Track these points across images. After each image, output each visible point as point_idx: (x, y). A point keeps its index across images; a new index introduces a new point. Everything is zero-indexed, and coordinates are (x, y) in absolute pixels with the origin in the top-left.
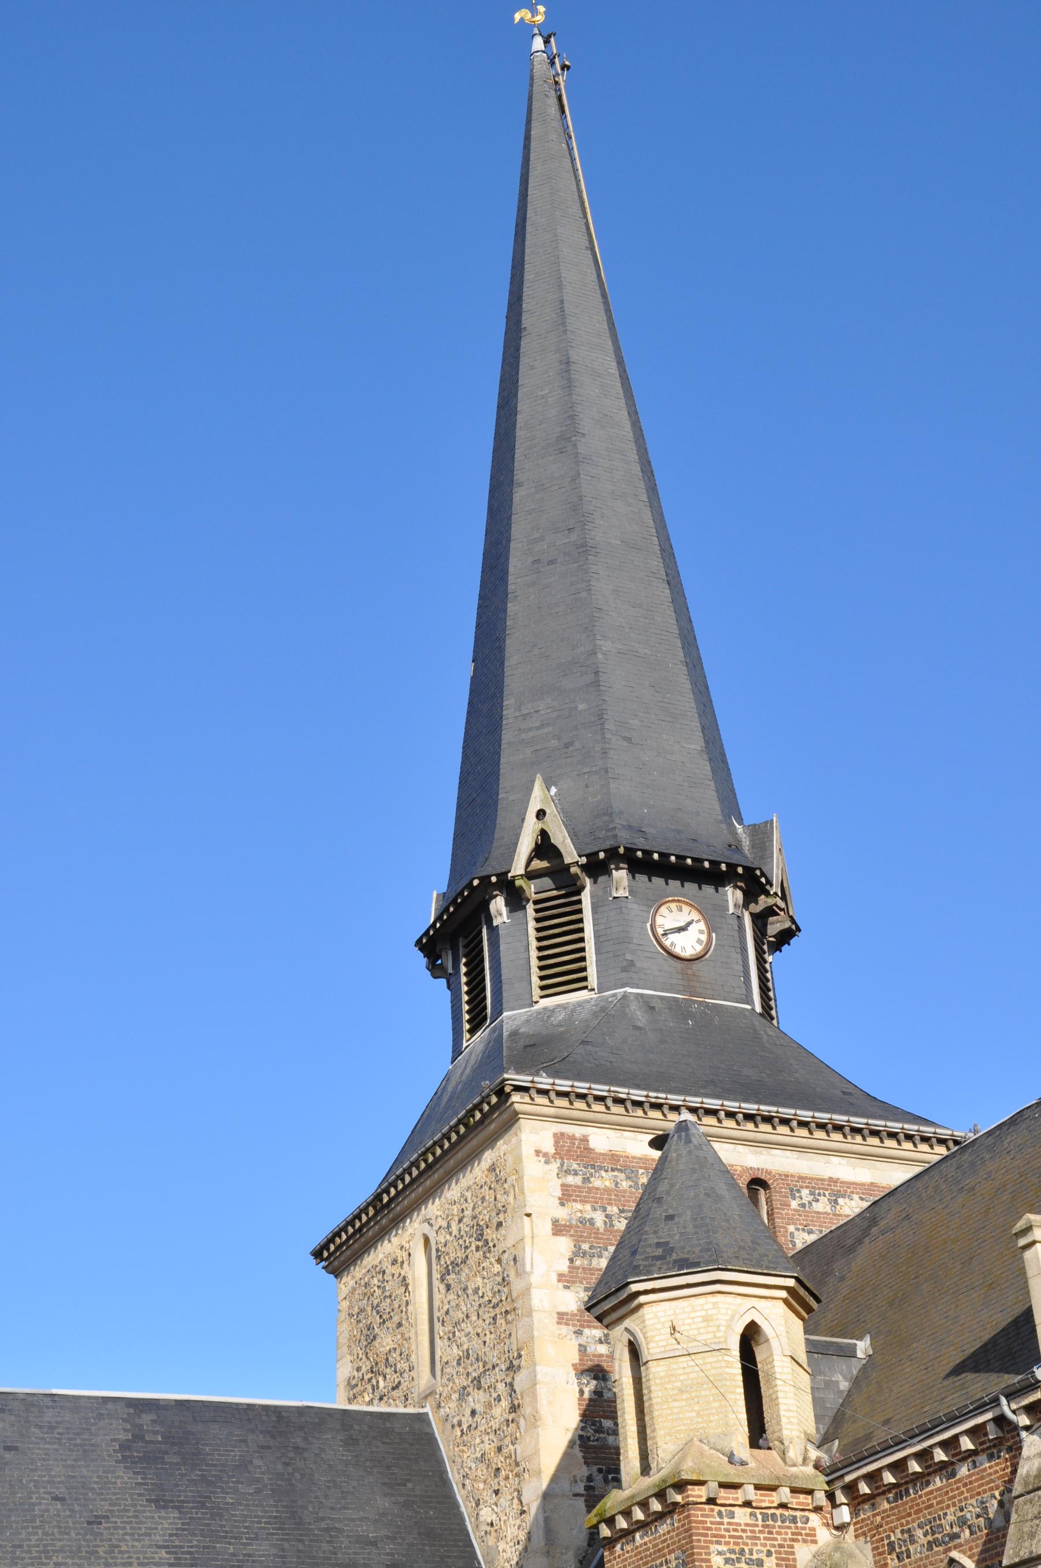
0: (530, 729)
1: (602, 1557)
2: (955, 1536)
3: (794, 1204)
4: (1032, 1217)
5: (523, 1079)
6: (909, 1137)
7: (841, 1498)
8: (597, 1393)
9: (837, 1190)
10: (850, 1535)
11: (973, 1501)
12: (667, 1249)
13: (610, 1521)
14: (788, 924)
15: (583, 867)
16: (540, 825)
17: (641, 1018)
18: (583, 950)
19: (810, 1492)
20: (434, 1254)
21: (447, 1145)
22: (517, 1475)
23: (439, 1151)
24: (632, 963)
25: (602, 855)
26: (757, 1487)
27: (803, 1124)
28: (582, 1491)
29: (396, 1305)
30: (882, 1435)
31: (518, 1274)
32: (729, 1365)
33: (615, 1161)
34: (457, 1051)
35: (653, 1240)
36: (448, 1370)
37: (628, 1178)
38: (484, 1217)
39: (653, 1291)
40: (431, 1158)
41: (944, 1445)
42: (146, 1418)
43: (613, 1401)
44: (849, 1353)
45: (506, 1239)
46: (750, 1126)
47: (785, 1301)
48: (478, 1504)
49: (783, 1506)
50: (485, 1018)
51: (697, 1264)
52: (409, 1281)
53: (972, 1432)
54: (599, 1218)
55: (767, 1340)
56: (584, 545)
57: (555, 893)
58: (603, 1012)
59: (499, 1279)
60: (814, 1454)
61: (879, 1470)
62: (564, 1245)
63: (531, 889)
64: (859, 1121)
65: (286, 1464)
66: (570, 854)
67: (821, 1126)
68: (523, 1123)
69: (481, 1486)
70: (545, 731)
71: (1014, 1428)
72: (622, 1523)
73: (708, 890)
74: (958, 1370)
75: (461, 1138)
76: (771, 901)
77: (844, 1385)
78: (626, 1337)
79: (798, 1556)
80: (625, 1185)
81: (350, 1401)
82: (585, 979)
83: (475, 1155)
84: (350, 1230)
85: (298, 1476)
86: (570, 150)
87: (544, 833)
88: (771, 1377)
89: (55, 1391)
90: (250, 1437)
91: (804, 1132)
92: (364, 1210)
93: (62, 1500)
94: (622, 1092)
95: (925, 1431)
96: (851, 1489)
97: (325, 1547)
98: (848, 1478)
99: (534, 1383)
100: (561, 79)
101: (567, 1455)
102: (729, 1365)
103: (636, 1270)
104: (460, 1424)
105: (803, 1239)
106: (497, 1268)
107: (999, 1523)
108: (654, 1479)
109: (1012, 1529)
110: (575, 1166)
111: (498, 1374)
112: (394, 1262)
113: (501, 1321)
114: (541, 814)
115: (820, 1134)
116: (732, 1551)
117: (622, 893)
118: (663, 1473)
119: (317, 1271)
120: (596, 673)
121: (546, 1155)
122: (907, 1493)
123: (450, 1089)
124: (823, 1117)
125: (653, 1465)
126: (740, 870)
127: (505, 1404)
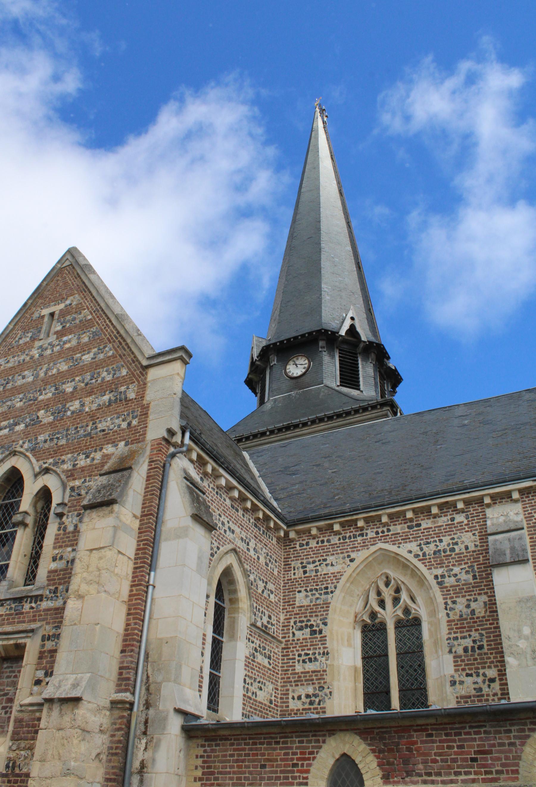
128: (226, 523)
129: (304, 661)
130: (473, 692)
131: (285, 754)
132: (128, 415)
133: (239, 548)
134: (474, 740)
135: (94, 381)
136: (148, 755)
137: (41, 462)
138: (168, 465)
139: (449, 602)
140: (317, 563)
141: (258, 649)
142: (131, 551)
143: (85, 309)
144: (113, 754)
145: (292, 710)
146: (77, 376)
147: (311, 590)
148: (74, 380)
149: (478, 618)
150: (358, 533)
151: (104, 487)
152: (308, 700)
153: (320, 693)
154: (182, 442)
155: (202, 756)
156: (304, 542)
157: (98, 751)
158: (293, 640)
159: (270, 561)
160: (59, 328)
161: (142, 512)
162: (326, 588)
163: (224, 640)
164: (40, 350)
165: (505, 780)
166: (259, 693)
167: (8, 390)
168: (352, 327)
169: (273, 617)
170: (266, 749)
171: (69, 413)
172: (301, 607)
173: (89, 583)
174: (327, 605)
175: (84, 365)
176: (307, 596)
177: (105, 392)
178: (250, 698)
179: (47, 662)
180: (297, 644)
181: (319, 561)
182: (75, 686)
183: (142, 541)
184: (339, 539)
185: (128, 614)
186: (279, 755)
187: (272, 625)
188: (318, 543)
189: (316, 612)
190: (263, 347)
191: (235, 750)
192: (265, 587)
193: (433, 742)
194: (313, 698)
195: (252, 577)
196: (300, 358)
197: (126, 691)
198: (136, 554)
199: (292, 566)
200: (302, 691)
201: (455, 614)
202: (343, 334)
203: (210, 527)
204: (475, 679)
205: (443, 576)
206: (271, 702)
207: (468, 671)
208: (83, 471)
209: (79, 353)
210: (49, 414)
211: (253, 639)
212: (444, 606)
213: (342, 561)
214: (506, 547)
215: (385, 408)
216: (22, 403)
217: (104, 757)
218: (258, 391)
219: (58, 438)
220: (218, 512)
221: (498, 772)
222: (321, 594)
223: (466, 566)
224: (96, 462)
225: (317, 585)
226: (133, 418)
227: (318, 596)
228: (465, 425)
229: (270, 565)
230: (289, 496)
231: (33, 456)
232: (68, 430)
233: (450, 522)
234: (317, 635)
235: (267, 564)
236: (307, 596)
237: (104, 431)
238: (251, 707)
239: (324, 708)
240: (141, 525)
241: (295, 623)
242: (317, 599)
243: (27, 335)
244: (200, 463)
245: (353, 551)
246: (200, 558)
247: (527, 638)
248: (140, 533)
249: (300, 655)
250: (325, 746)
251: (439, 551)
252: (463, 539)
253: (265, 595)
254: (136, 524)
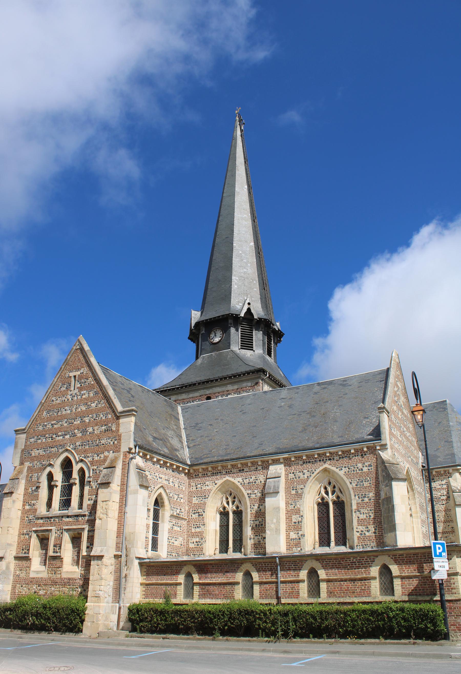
128: (157, 475)
129: (195, 527)
130: (257, 542)
131: (171, 571)
132: (113, 438)
133: (164, 484)
134: (225, 568)
135: (97, 418)
136: (128, 572)
137: (79, 456)
138: (130, 463)
139: (252, 505)
140: (202, 484)
141: (175, 524)
142: (118, 500)
143: (90, 378)
144: (116, 572)
145: (190, 548)
146: (90, 414)
147: (199, 497)
148: (89, 416)
149: (262, 512)
150: (219, 472)
151: (106, 475)
152: (197, 544)
153: (201, 541)
154: (135, 452)
155: (146, 572)
156: (197, 474)
157: (111, 571)
158: (191, 518)
159: (181, 484)
160: (79, 385)
161: (121, 483)
162: (205, 496)
163: (159, 522)
164: (71, 396)
165: (231, 580)
166: (175, 542)
167: (59, 416)
168: (249, 309)
169: (182, 509)
170: (166, 570)
171: (88, 433)
172: (195, 504)
173: (103, 514)
174: (205, 503)
175: (93, 409)
176: (197, 499)
177: (103, 425)
178: (171, 545)
179: (90, 540)
180: (193, 520)
181: (203, 483)
182: (101, 551)
183: (121, 495)
184: (211, 474)
185: (118, 524)
186: (170, 571)
187: (182, 512)
188: (202, 475)
189: (200, 506)
190: (196, 323)
191: (156, 570)
192: (178, 497)
193: (214, 568)
194: (198, 543)
195: (171, 495)
196: (218, 330)
197: (119, 551)
198: (120, 501)
199: (192, 485)
200: (195, 540)
201: (254, 510)
202: (243, 316)
203: (147, 488)
204: (258, 537)
205: (250, 494)
206: (181, 545)
207: (256, 534)
208: (97, 462)
209: (90, 402)
210: (80, 432)
211: (172, 521)
212: (250, 507)
213: (211, 484)
214: (272, 485)
215: (259, 373)
216: (67, 424)
217: (113, 573)
218: (196, 342)
219: (85, 445)
220: (154, 472)
221: (230, 578)
222: (203, 499)
223: (260, 490)
224: (101, 459)
225: (201, 494)
226: (115, 440)
227: (201, 499)
228: (281, 407)
229: (181, 486)
230: (194, 446)
231: (75, 452)
232: (89, 441)
233: (255, 470)
234: (201, 517)
235: (179, 487)
236: (197, 499)
237: (103, 444)
238: (171, 549)
239: (203, 547)
240: (121, 489)
241: (192, 511)
242: (201, 500)
243: (64, 386)
244: (144, 456)
245: (216, 480)
246: (144, 500)
247: (274, 524)
248: (120, 492)
249: (194, 525)
250: (183, 569)
251: (250, 482)
252: (260, 478)
253: (178, 500)
254: (119, 488)
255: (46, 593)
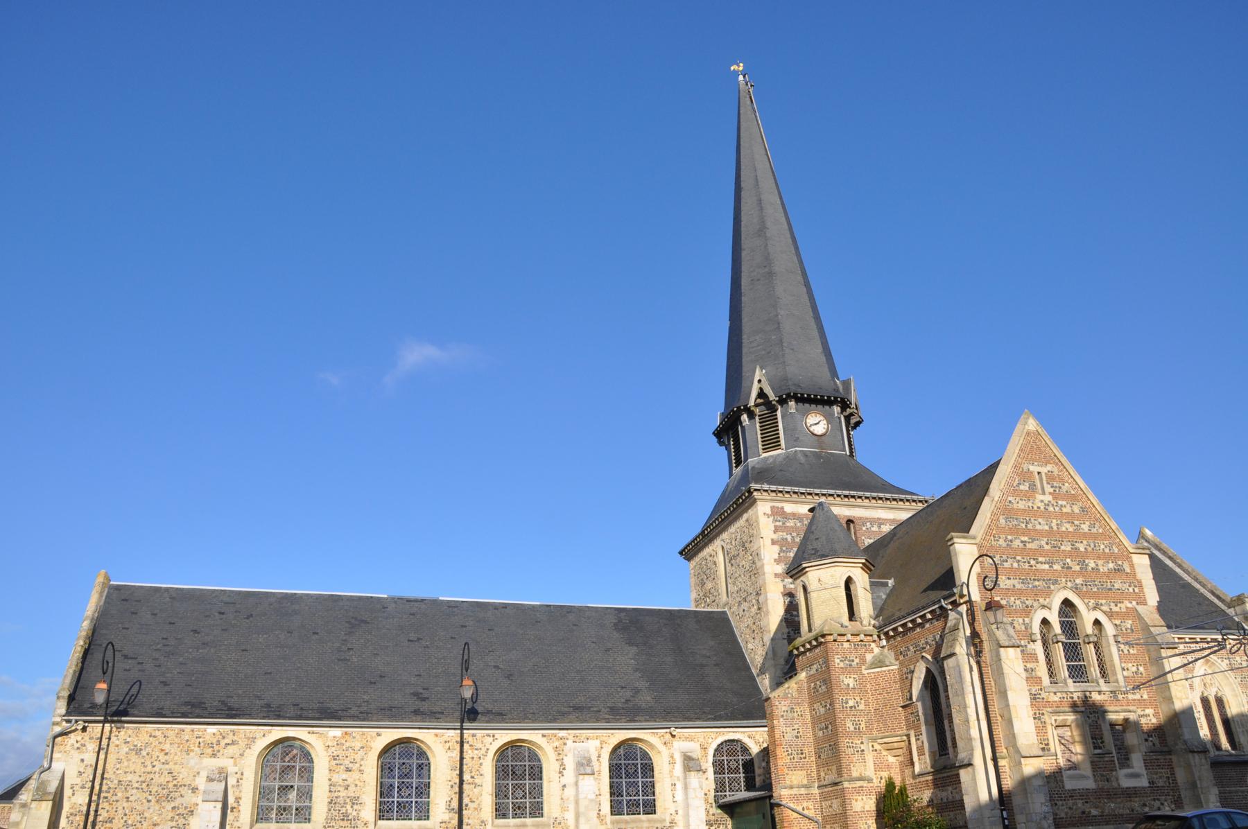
0: (753, 347)
1: (794, 660)
2: (924, 648)
3: (864, 528)
4: (953, 534)
5: (758, 486)
6: (908, 501)
7: (883, 637)
8: (791, 602)
9: (880, 522)
10: (886, 650)
11: (931, 636)
12: (816, 551)
13: (797, 649)
14: (858, 419)
15: (777, 401)
16: (759, 386)
17: (803, 460)
18: (778, 434)
19: (871, 635)
20: (726, 552)
21: (729, 512)
22: (761, 632)
23: (726, 514)
24: (798, 438)
25: (784, 396)
26: (852, 635)
27: (867, 498)
28: (786, 637)
29: (712, 571)
30: (898, 614)
31: (759, 560)
32: (841, 592)
33: (794, 516)
34: (731, 474)
35: (811, 547)
36: (733, 595)
37: (800, 522)
38: (745, 538)
39: (811, 566)
40: (723, 517)
41: (920, 617)
42: (622, 615)
43: (797, 605)
44: (886, 585)
45: (754, 547)
46: (846, 499)
47: (861, 568)
48: (747, 642)
49: (861, 641)
50: (741, 462)
51: (827, 556)
52: (717, 562)
53: (931, 612)
54: (789, 538)
55: (855, 582)
56: (771, 273)
57: (766, 412)
58: (789, 459)
59: (752, 561)
60: (873, 622)
61: (897, 627)
62: (776, 548)
63: (757, 411)
64: (888, 496)
65: (675, 630)
66: (772, 397)
67: (874, 498)
68: (759, 503)
69: (748, 636)
70: (759, 348)
71: (946, 610)
72: (802, 649)
73: (827, 407)
74: (925, 591)
75: (734, 509)
76: (851, 411)
77: (884, 597)
78: (802, 583)
79: (867, 658)
80: (799, 524)
81: (696, 607)
82: (780, 445)
83: (740, 515)
84: (693, 544)
85: (679, 634)
86: (756, 117)
87: (761, 389)
88: (856, 596)
89: (589, 605)
90: (661, 621)
91: (867, 501)
92: (698, 537)
93: (595, 643)
94: (796, 489)
95: (913, 612)
96: (886, 634)
97: (691, 659)
98: (885, 630)
99: (766, 600)
100: (751, 90)
101: (780, 625)
102: (841, 592)
103: (805, 559)
104: (739, 614)
105: (868, 542)
106: (751, 558)
107: (940, 643)
108: (813, 633)
109: (944, 644)
110: (779, 518)
111: (753, 596)
112: (711, 556)
113: (753, 577)
114: (760, 381)
115: (874, 501)
116: (843, 657)
117: (793, 411)
118: (816, 631)
119: (681, 559)
120: (779, 324)
121: (768, 515)
122: (907, 634)
123: (729, 489)
124: (874, 495)
125: (813, 629)
126: (839, 399)
127: (755, 607)
255: (1102, 812)
